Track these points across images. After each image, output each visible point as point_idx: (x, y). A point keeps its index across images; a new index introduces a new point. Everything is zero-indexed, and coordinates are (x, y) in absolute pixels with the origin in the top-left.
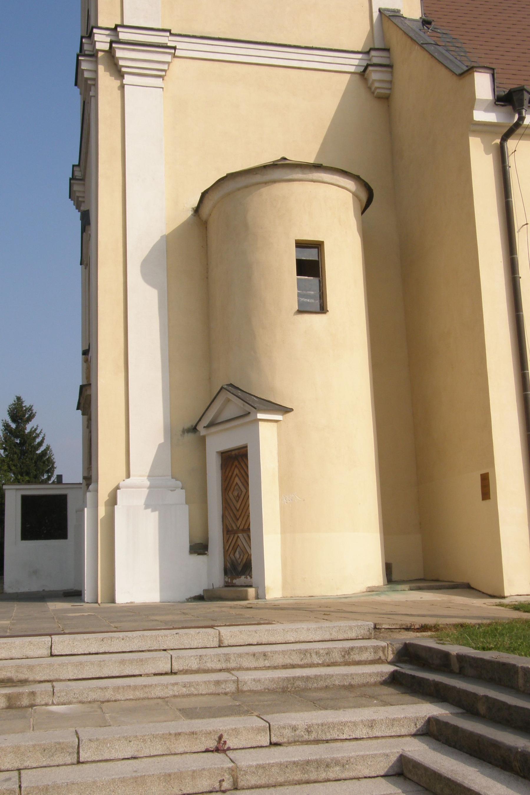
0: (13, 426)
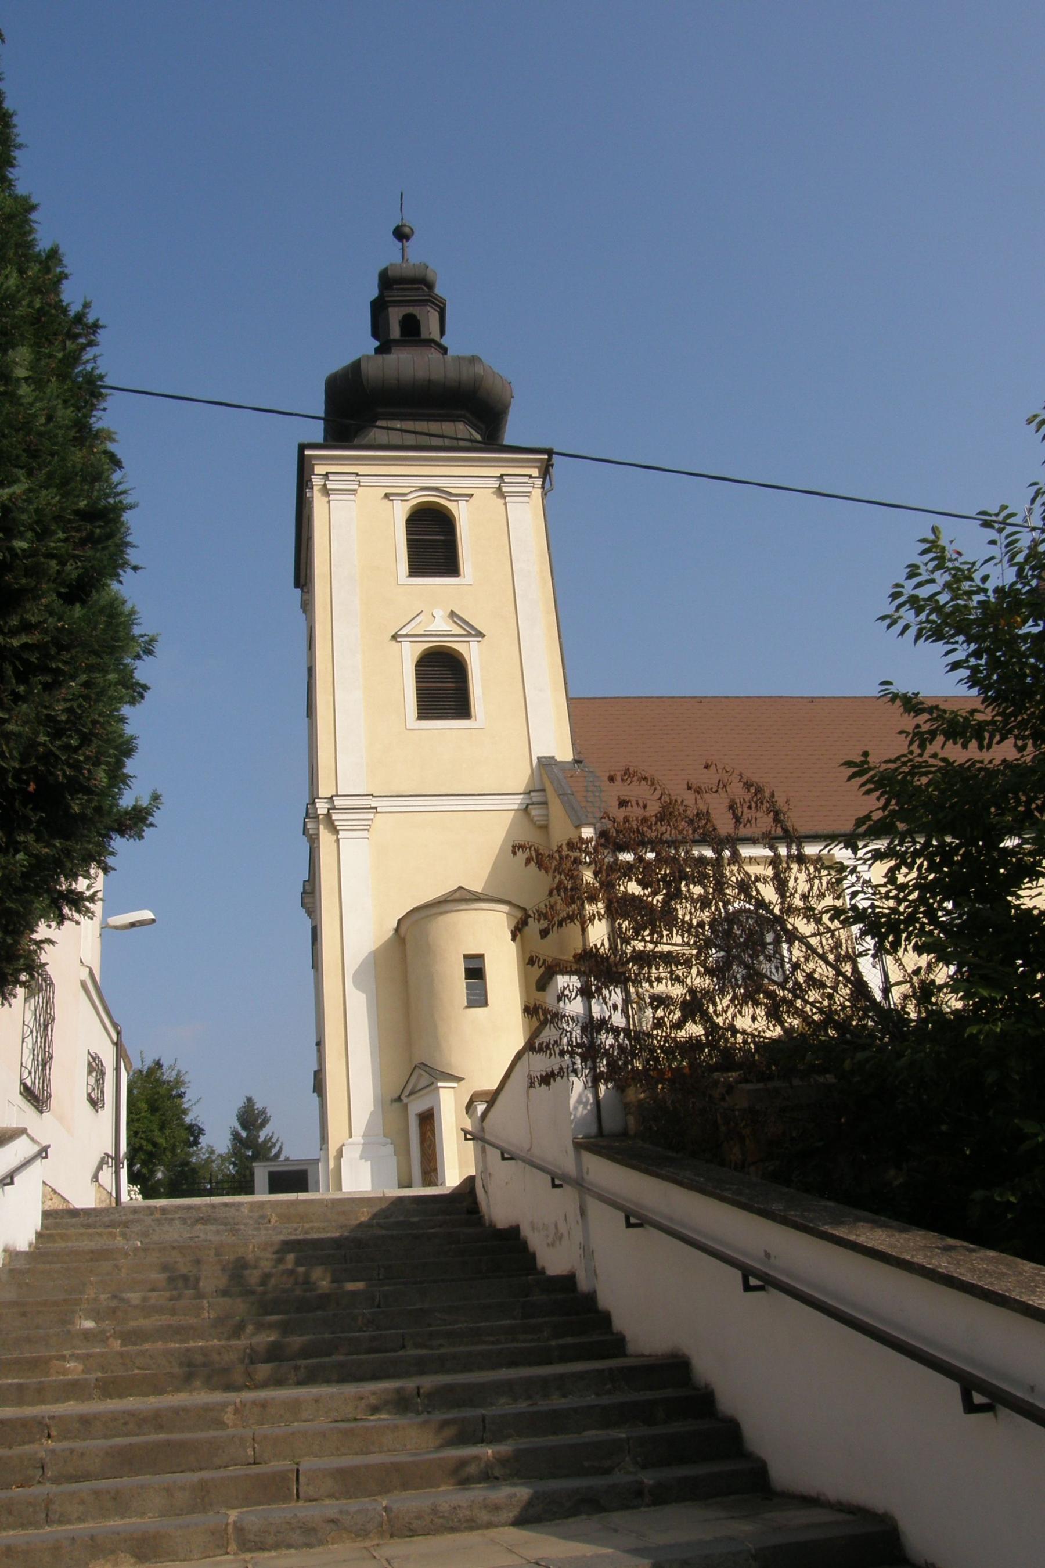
0: (244, 1134)
